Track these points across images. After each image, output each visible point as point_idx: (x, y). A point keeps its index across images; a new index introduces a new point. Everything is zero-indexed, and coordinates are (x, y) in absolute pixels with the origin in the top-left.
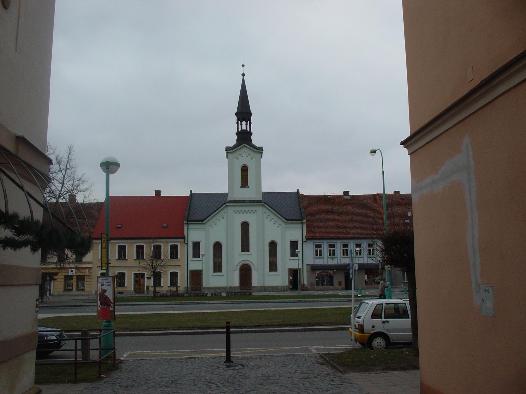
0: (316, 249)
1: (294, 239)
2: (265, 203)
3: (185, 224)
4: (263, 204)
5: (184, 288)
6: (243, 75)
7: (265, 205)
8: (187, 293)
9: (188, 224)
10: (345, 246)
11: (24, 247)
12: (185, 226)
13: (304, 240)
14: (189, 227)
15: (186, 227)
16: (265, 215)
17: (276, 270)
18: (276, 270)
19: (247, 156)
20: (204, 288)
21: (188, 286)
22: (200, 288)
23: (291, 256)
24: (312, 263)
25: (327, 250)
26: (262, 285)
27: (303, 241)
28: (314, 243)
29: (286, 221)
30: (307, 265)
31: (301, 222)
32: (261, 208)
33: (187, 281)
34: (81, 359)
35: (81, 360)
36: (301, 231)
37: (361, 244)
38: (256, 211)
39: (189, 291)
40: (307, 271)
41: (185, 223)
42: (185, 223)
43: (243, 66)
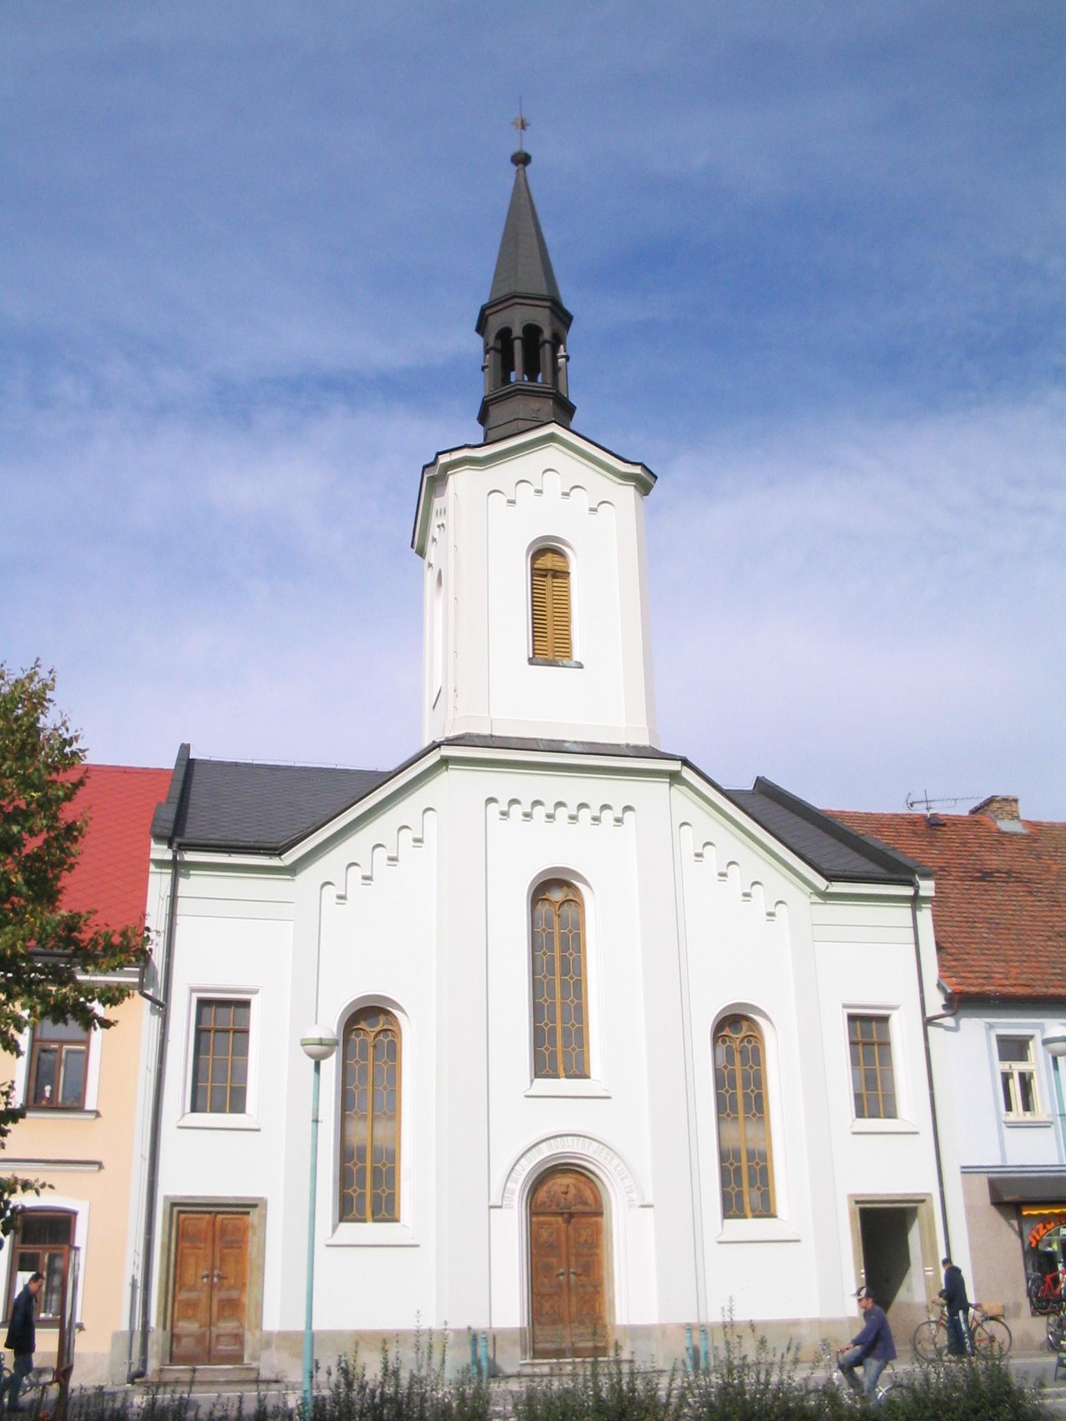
0: (1005, 1066)
1: (869, 998)
2: (685, 762)
3: (152, 868)
4: (675, 766)
5: (116, 1336)
6: (522, 159)
7: (687, 774)
8: (136, 1377)
9: (178, 868)
10: (1013, 1048)
11: (78, 1023)
12: (152, 878)
13: (936, 1003)
14: (181, 891)
15: (158, 883)
16: (689, 841)
17: (766, 1210)
18: (766, 1210)
19: (566, 494)
20: (268, 1341)
21: (146, 1323)
22: (238, 1338)
23: (860, 1114)
24: (990, 1157)
25: (993, 1075)
26: (693, 1320)
27: (929, 1015)
28: (991, 1026)
29: (821, 883)
30: (967, 1171)
31: (909, 891)
32: (660, 787)
33: (140, 1284)
34: (550, 386)
35: (550, 388)
36: (913, 947)
37: (1032, 1037)
38: (628, 808)
39: (153, 1364)
40: (970, 1210)
41: (153, 856)
42: (153, 856)
43: (523, 126)
